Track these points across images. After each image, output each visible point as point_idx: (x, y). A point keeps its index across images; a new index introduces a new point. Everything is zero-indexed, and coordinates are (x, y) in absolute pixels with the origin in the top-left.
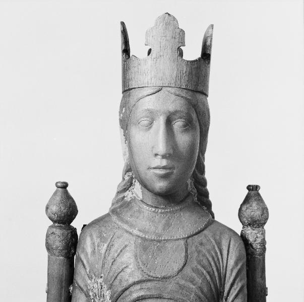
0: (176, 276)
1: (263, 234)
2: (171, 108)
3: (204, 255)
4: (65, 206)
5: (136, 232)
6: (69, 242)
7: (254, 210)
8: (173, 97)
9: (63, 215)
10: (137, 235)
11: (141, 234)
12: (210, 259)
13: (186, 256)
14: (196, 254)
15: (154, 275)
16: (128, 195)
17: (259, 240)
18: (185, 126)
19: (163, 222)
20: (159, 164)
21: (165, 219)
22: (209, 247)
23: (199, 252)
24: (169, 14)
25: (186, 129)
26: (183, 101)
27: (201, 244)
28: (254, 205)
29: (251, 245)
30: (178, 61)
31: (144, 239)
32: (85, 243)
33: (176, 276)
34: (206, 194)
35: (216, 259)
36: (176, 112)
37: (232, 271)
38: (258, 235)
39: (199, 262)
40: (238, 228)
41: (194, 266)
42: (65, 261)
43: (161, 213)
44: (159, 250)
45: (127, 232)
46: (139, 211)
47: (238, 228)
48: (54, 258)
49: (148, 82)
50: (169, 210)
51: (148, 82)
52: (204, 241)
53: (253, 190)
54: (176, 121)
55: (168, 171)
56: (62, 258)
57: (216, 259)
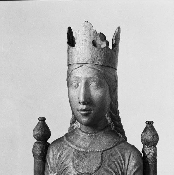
0: (94, 173)
1: (155, 150)
2: (88, 76)
3: (113, 162)
4: (42, 131)
5: (74, 147)
6: (44, 152)
7: (149, 136)
8: (90, 69)
9: (40, 136)
10: (75, 149)
11: (77, 148)
12: (117, 164)
13: (102, 161)
14: (108, 161)
15: (82, 172)
16: (75, 125)
17: (151, 154)
18: (97, 86)
19: (90, 141)
20: (82, 108)
21: (91, 140)
22: (116, 157)
23: (110, 159)
24: (88, 22)
25: (98, 88)
26: (95, 72)
27: (112, 155)
28: (148, 133)
29: (147, 157)
30: (92, 49)
31: (79, 151)
32: (49, 153)
33: (94, 173)
34: (121, 127)
35: (120, 164)
36: (90, 78)
37: (131, 171)
38: (151, 151)
39: (109, 166)
40: (140, 147)
41: (105, 168)
42: (42, 162)
43: (89, 136)
44: (86, 157)
45: (70, 146)
46: (78, 135)
47: (140, 147)
48: (36, 160)
49: (76, 61)
50: (93, 135)
51: (76, 61)
52: (114, 153)
53: (150, 124)
54: (92, 83)
55: (88, 112)
56: (40, 160)
57: (120, 164)
